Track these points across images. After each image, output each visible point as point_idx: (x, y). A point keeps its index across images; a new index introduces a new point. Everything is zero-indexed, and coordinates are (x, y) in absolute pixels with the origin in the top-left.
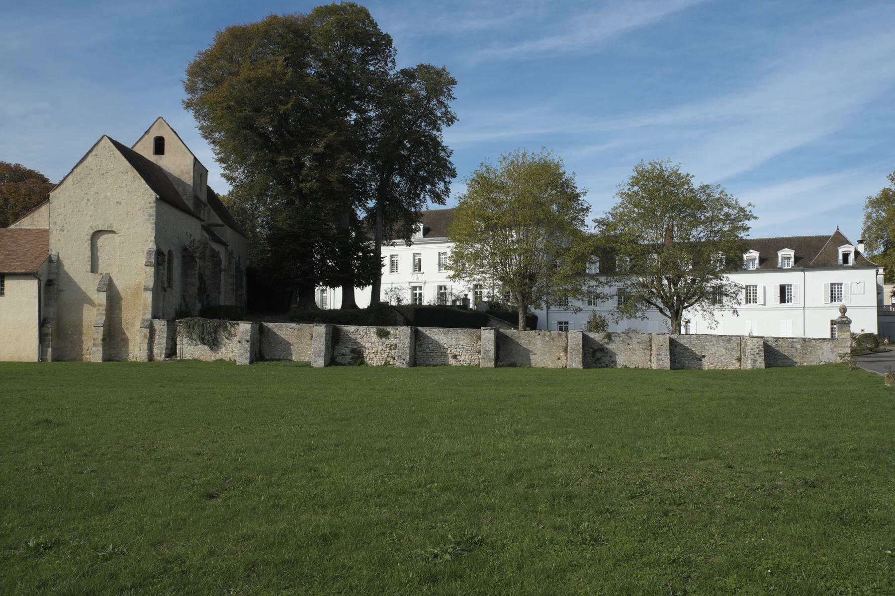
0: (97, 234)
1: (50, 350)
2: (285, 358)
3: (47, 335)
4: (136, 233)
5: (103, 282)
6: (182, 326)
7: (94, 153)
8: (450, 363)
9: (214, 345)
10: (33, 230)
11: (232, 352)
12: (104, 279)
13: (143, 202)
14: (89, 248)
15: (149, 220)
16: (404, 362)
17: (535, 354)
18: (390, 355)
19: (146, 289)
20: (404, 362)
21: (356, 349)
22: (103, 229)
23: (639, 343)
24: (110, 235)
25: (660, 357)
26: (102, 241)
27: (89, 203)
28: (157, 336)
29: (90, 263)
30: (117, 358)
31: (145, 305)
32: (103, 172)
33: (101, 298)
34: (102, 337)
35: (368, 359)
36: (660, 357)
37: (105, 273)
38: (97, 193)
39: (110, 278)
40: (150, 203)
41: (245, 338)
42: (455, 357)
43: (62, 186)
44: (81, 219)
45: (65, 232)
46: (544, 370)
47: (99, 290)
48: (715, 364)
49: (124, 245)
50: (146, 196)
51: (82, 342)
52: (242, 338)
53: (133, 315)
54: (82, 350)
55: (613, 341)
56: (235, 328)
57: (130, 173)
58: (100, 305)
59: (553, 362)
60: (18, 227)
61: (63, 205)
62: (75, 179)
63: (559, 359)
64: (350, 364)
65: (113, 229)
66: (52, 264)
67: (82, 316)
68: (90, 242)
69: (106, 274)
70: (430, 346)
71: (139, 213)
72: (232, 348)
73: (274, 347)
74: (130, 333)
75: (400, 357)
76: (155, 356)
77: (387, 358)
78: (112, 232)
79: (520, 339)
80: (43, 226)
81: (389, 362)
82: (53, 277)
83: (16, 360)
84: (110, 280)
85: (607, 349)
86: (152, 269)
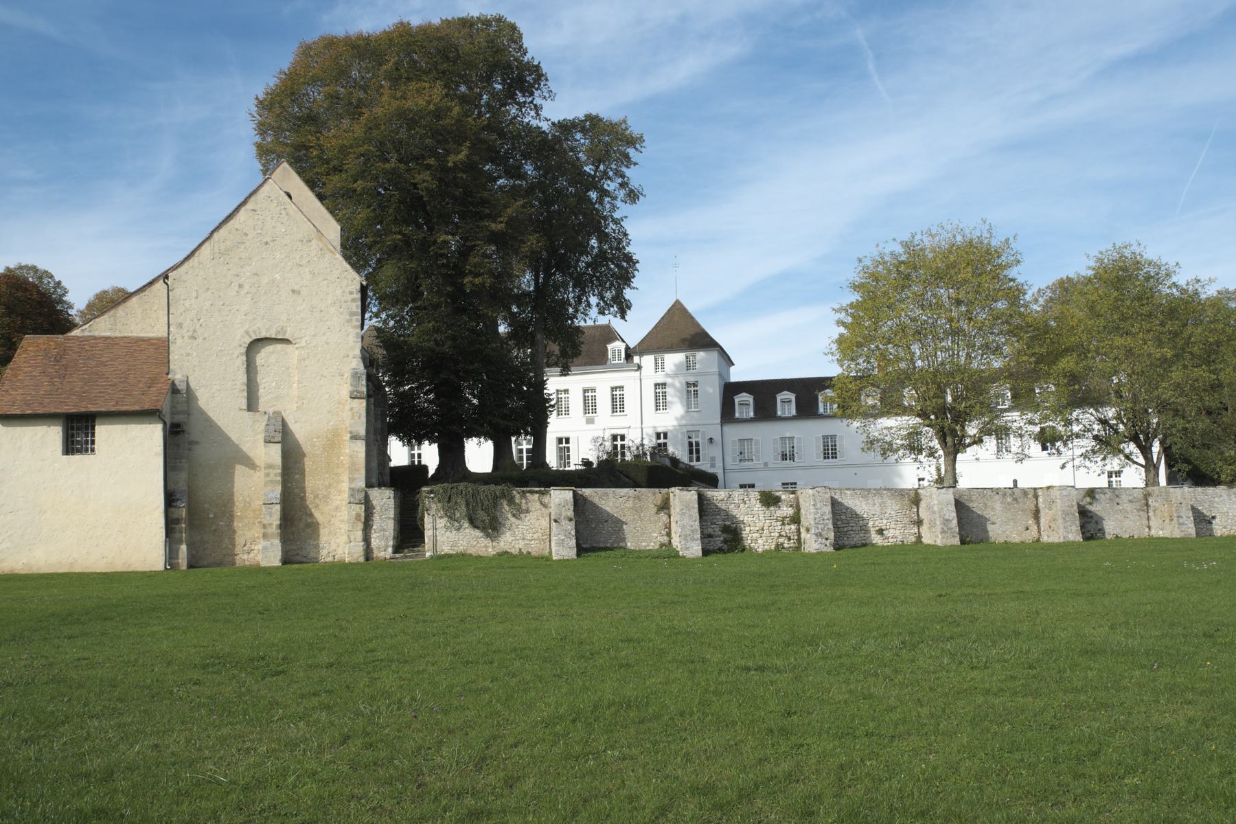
0: (257, 344)
1: (184, 547)
2: (616, 545)
3: (177, 521)
4: (327, 343)
5: (272, 428)
6: (433, 498)
7: (249, 206)
8: (874, 542)
9: (492, 527)
10: (116, 338)
11: (523, 539)
12: (272, 421)
13: (339, 292)
14: (243, 369)
15: (349, 321)
16: (828, 542)
17: (993, 523)
18: (783, 533)
19: (354, 437)
20: (828, 542)
21: (729, 526)
22: (268, 336)
23: (1131, 501)
24: (279, 346)
25: (1181, 520)
26: (264, 356)
27: (243, 292)
28: (376, 517)
29: (245, 394)
30: (299, 558)
31: (353, 464)
32: (268, 239)
33: (274, 454)
34: (278, 522)
35: (749, 542)
36: (1181, 520)
37: (271, 411)
38: (256, 274)
39: (283, 420)
40: (351, 293)
41: (564, 514)
42: (880, 532)
43: (191, 261)
44: (228, 318)
45: (200, 340)
46: (929, 545)
47: (268, 441)
48: (1229, 527)
49: (307, 363)
50: (345, 282)
51: (234, 532)
52: (560, 515)
53: (327, 483)
54: (234, 546)
55: (1097, 500)
56: (526, 499)
57: (314, 242)
58: (270, 466)
59: (1020, 534)
60: (86, 334)
61: (194, 294)
62: (216, 250)
63: (1027, 529)
64: (721, 550)
65: (287, 337)
66: (179, 395)
67: (233, 486)
68: (244, 358)
69: (274, 413)
70: (843, 517)
71: (333, 310)
72: (523, 533)
73: (595, 529)
74: (322, 513)
75: (820, 535)
76: (375, 551)
77: (778, 537)
78: (286, 341)
79: (972, 501)
80: (157, 330)
81: (782, 544)
82: (179, 418)
83: (120, 569)
84: (284, 424)
85: (1091, 512)
86: (364, 403)
